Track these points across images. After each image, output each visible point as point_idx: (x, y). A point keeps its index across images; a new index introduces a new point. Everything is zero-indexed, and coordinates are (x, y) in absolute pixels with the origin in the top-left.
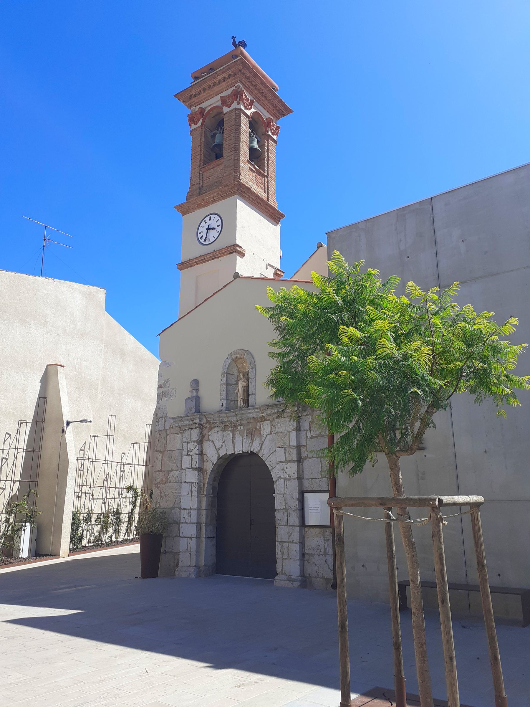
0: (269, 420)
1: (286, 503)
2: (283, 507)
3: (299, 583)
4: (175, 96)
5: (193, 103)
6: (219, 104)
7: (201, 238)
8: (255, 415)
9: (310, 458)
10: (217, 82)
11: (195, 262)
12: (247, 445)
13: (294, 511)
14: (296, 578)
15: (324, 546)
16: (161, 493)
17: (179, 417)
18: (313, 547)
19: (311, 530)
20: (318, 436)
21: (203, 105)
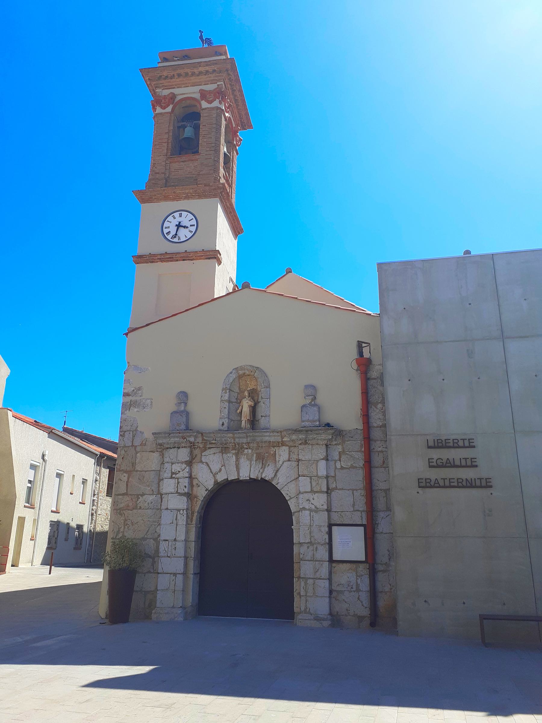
0: (287, 446)
1: (311, 537)
2: (308, 540)
3: (330, 622)
4: (141, 70)
5: (161, 85)
6: (197, 96)
7: (168, 233)
8: (272, 439)
10: (197, 72)
11: (160, 259)
12: (257, 472)
13: (322, 545)
15: (357, 582)
16: (125, 520)
17: (165, 433)
21: (176, 91)
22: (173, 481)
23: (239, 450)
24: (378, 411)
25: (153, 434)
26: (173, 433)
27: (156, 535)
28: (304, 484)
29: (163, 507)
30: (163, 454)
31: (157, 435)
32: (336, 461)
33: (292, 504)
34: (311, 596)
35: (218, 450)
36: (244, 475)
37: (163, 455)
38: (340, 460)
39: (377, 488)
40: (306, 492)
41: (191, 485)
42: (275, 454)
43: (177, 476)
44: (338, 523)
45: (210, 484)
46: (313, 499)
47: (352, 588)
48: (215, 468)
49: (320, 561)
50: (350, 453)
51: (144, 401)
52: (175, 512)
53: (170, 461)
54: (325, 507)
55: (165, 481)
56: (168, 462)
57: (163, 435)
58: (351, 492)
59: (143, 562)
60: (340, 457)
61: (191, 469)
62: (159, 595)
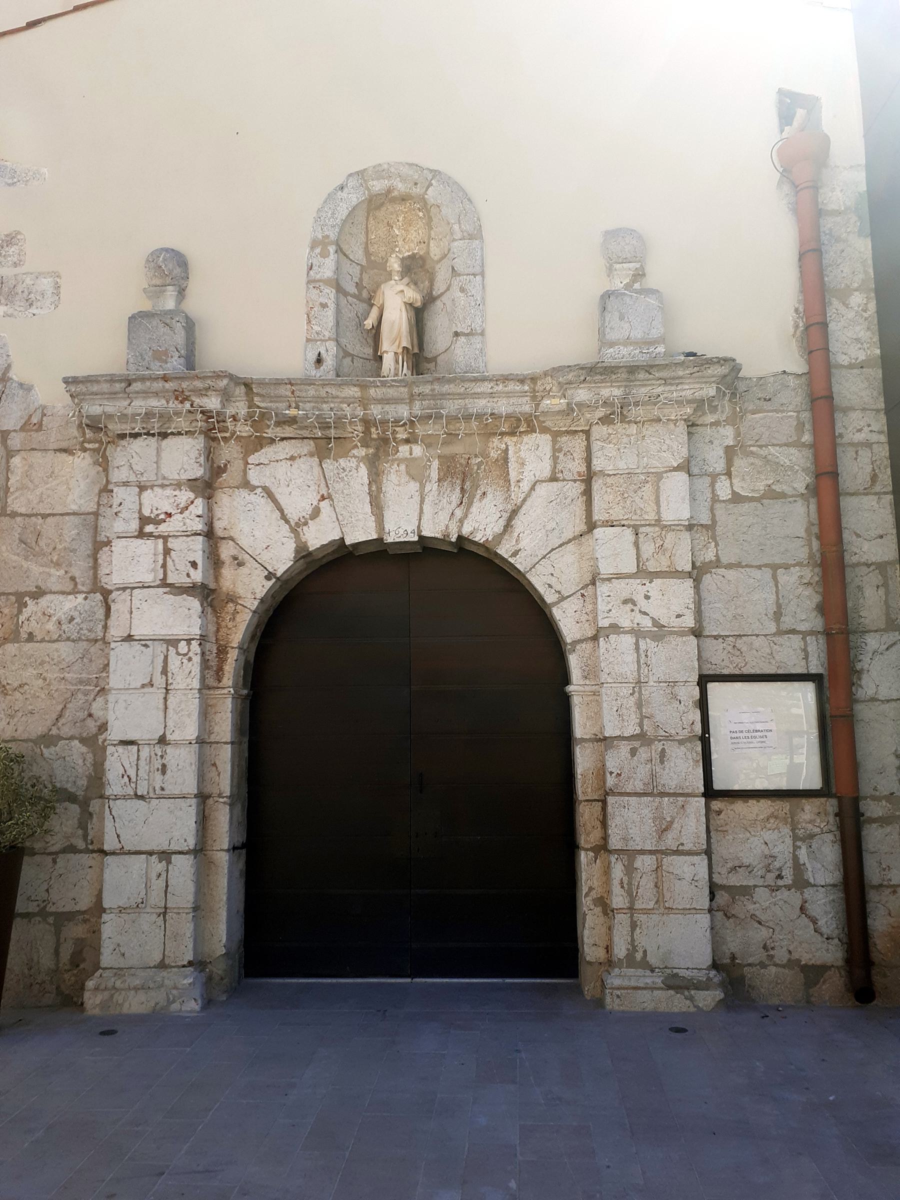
0: (545, 430)
1: (642, 718)
2: (632, 729)
3: (719, 994)
8: (503, 407)
9: (729, 566)
12: (443, 517)
13: (681, 742)
14: (702, 976)
15: (795, 858)
17: (112, 379)
18: (746, 862)
19: (739, 806)
20: (763, 497)
22: (146, 547)
23: (380, 443)
24: (851, 315)
25: (66, 381)
26: (143, 379)
27: (92, 726)
28: (613, 550)
29: (116, 630)
30: (104, 457)
31: (81, 388)
32: (714, 477)
33: (569, 622)
34: (647, 906)
36: (401, 528)
37: (104, 464)
38: (729, 474)
39: (855, 559)
40: (620, 576)
41: (215, 561)
42: (506, 460)
43: (163, 528)
44: (726, 672)
45: (283, 560)
46: (647, 597)
48: (298, 504)
49: (675, 795)
50: (763, 452)
51: (28, 281)
52: (161, 648)
53: (133, 478)
54: (689, 621)
55: (118, 546)
57: (105, 387)
58: (768, 573)
59: (46, 817)
60: (729, 463)
61: (210, 509)
62: (110, 927)
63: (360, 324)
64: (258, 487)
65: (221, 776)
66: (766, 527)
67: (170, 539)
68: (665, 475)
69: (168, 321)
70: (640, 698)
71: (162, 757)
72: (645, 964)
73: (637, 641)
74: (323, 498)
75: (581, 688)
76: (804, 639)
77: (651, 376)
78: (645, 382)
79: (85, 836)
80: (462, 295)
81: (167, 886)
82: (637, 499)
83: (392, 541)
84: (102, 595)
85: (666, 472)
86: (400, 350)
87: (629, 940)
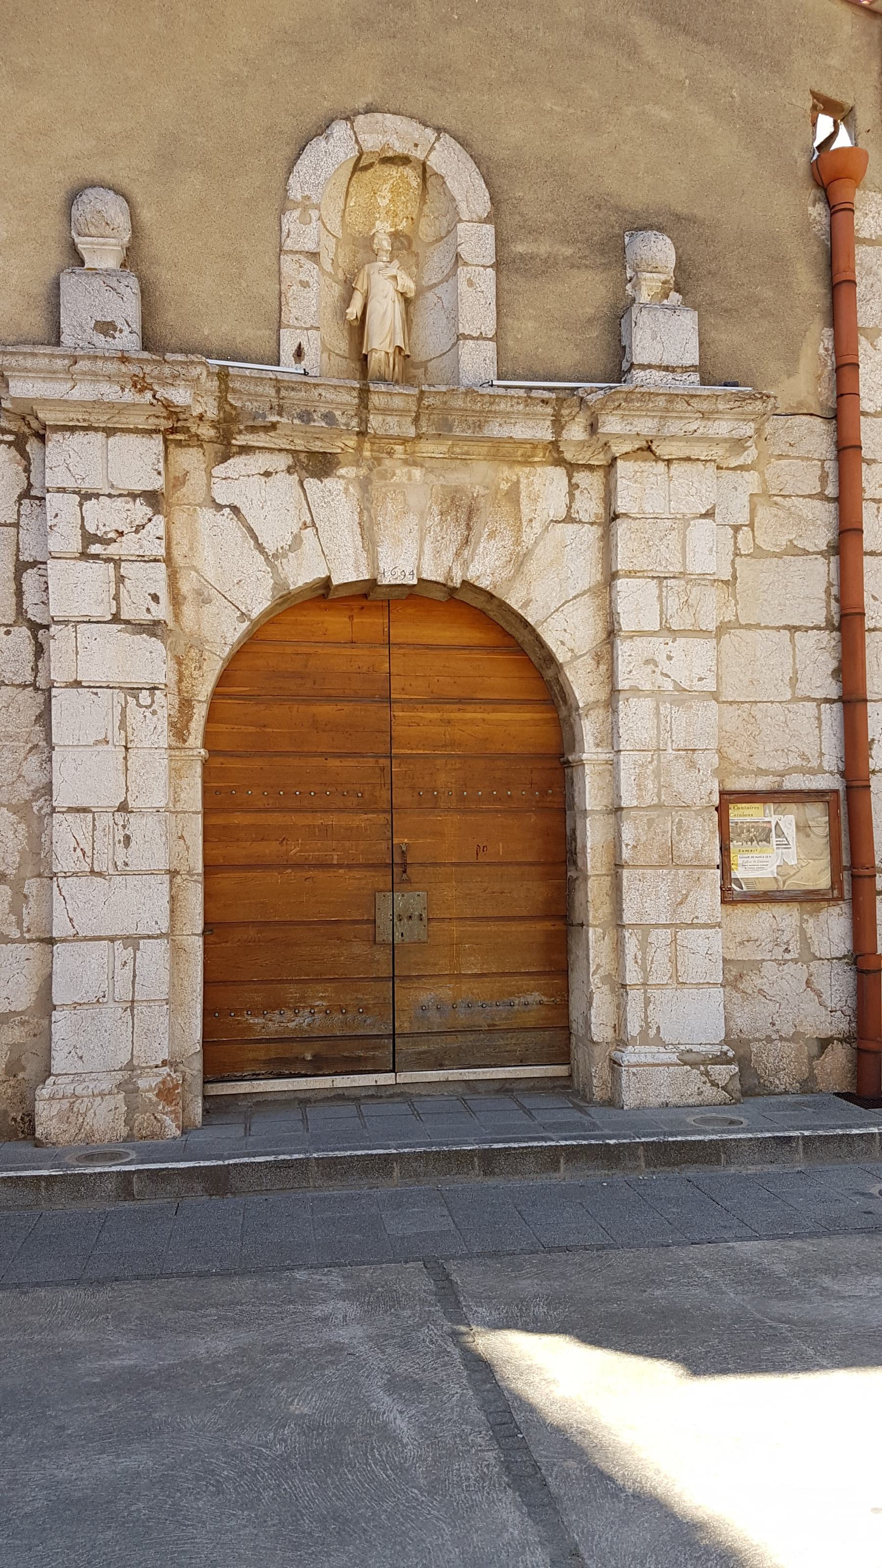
2: (650, 799)
9: (748, 627)
12: (448, 557)
13: (698, 813)
15: (803, 931)
18: (754, 936)
20: (785, 553)
35: (282, 461)
40: (642, 634)
46: (670, 658)
47: (787, 951)
56: (62, 490)
63: (344, 314)
64: (226, 506)
65: (191, 851)
66: (787, 586)
67: (123, 564)
68: (692, 523)
69: (115, 284)
70: (658, 766)
71: (124, 826)
72: (659, 1041)
73: (658, 705)
74: (305, 526)
75: (595, 757)
76: (819, 705)
77: (690, 408)
78: (682, 414)
79: (19, 923)
80: (470, 289)
81: (134, 976)
82: (663, 548)
83: (386, 583)
84: (30, 629)
85: (694, 518)
86: (391, 351)
87: (643, 1017)
